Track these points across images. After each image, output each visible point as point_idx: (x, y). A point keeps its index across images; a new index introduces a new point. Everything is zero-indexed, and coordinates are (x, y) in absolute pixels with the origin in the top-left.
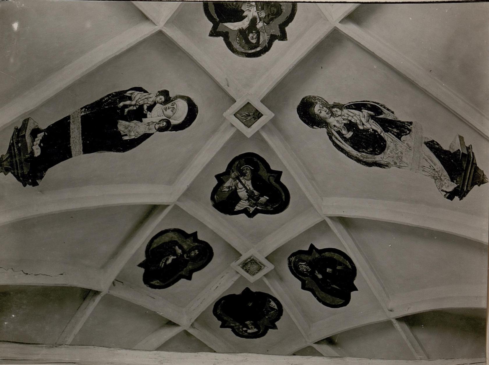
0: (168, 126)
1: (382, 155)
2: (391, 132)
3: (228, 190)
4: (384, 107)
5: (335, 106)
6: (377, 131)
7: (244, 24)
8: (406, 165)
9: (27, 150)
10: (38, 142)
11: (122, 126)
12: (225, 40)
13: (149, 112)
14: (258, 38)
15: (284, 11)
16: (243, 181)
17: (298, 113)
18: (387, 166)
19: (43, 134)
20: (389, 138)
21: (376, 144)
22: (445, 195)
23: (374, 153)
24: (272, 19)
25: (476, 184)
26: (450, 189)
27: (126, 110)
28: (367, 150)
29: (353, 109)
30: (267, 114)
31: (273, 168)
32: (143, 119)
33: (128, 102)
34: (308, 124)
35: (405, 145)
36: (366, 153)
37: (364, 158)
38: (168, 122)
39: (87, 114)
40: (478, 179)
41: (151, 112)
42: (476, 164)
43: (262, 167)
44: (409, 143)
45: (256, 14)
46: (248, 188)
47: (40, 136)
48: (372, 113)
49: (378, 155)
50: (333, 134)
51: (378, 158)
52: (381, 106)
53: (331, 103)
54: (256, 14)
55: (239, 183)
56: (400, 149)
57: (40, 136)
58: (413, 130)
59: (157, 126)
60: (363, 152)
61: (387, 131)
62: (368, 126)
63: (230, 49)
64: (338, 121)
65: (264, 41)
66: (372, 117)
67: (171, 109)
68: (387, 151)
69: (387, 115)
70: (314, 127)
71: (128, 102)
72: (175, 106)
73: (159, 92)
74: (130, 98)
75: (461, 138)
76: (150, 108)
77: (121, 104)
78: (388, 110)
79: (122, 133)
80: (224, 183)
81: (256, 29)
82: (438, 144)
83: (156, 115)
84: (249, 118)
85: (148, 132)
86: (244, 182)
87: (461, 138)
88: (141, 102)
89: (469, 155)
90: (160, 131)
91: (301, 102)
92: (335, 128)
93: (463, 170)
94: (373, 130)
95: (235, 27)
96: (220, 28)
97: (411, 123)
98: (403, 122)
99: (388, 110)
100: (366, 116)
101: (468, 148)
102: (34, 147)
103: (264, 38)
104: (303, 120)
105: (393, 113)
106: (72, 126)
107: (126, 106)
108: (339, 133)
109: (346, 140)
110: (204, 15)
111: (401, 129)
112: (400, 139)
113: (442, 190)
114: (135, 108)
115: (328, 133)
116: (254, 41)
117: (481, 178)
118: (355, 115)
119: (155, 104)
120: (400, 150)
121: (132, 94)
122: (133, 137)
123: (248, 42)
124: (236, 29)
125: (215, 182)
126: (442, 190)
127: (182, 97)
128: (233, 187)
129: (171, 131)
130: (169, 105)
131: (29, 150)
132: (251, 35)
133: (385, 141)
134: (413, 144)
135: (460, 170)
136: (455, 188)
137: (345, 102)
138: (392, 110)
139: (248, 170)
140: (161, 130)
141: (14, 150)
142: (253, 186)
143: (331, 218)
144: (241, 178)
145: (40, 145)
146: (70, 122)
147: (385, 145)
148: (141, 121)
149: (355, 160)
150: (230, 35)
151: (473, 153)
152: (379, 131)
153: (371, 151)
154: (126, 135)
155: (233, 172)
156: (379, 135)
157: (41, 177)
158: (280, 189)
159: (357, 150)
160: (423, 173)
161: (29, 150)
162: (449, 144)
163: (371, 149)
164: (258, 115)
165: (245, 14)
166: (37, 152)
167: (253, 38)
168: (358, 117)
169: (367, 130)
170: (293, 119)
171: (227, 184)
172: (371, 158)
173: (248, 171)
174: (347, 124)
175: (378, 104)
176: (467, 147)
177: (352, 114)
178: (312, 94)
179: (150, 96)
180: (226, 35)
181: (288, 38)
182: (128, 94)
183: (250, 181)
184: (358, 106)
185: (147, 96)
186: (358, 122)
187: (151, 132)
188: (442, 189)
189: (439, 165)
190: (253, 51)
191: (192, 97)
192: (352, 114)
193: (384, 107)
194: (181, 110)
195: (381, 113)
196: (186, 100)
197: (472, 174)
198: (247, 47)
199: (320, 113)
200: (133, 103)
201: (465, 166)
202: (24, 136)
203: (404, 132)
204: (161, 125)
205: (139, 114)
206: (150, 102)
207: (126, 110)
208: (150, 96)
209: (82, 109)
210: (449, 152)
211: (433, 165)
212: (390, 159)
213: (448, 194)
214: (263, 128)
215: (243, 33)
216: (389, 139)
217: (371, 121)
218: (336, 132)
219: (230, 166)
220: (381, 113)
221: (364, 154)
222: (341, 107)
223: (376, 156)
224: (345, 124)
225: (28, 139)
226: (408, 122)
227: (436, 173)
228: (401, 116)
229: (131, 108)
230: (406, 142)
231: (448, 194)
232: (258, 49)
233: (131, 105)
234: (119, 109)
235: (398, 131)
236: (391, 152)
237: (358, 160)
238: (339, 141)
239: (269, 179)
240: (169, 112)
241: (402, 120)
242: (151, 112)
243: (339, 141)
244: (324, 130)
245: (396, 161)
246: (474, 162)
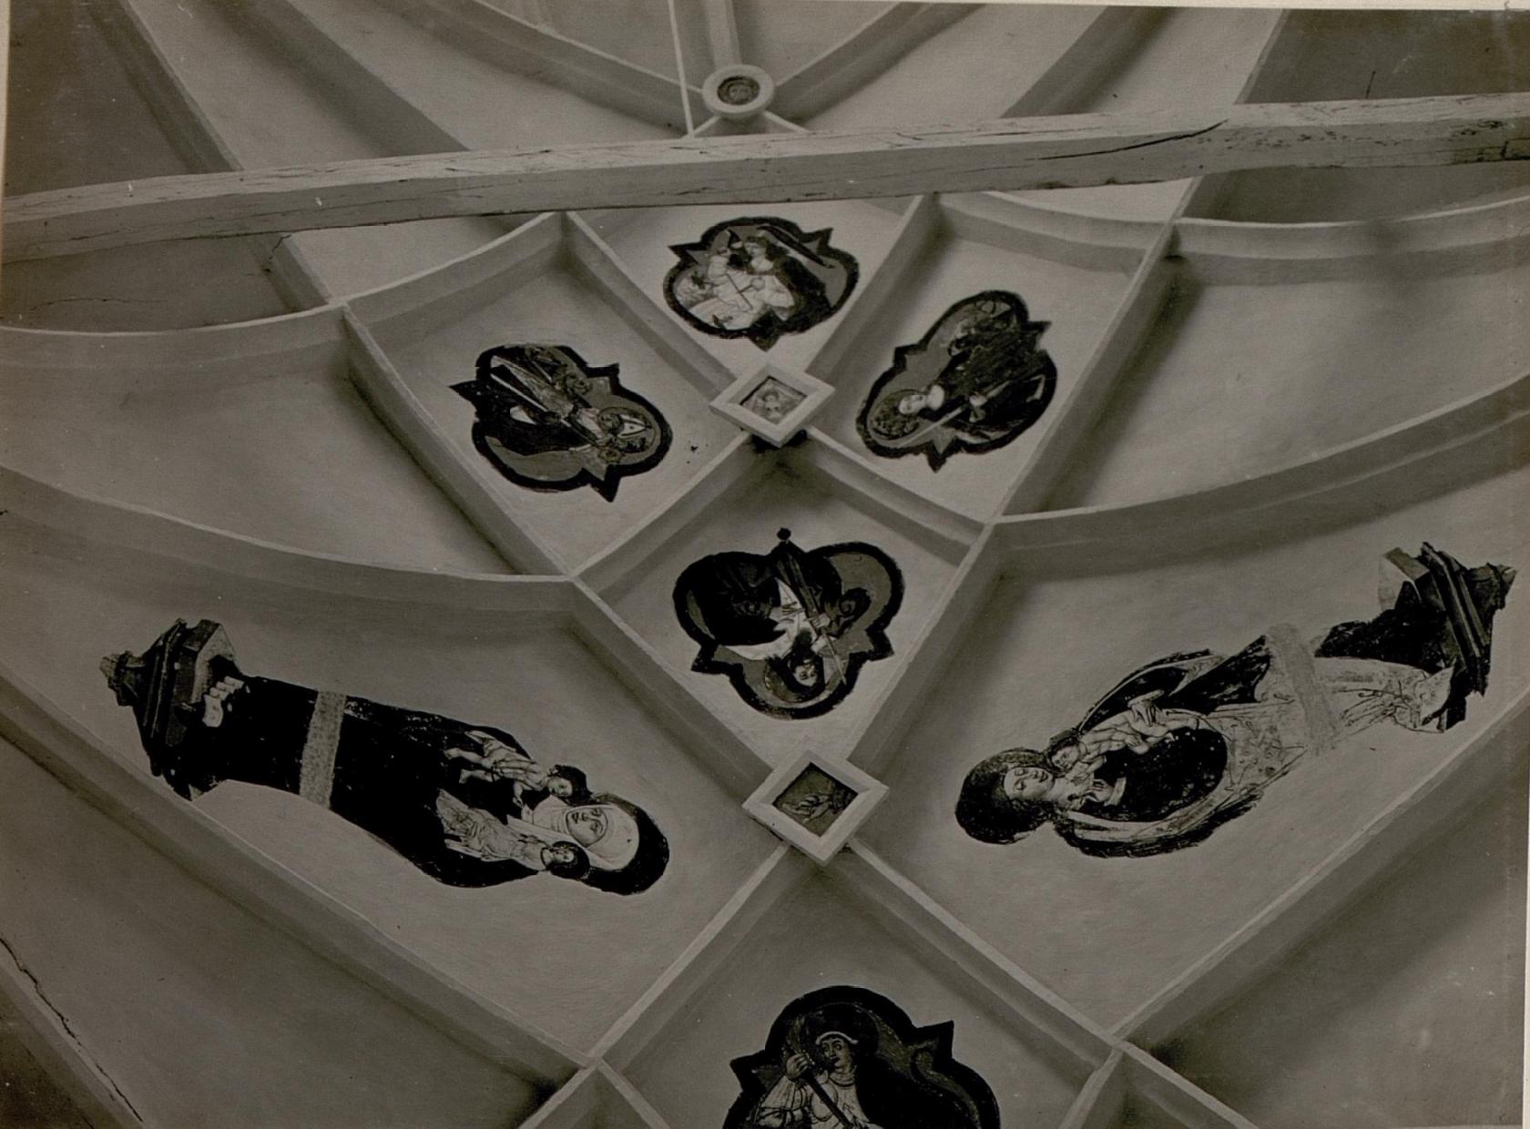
0: (577, 868)
1: (1225, 781)
2: (1223, 703)
3: (777, 1123)
4: (1182, 658)
5: (1058, 745)
6: (1186, 729)
7: (781, 647)
8: (1300, 751)
9: (190, 693)
10: (224, 696)
11: (448, 807)
12: (733, 682)
13: (526, 808)
14: (820, 672)
15: (874, 599)
16: (827, 1088)
17: (962, 824)
18: (1252, 798)
19: (239, 684)
20: (1224, 721)
21: (1198, 760)
22: (1439, 727)
23: (1202, 791)
24: (848, 624)
25: (1492, 610)
26: (1443, 695)
27: (465, 774)
28: (1178, 797)
29: (1103, 718)
30: (870, 792)
31: (918, 1022)
32: (510, 818)
33: (472, 756)
34: (995, 840)
35: (1272, 700)
36: (1180, 807)
37: (1182, 824)
38: (581, 855)
39: (358, 720)
40: (1489, 590)
41: (532, 807)
42: (1462, 568)
43: (885, 1030)
44: (1281, 690)
45: (807, 625)
46: (850, 1119)
47: (231, 684)
48: (1157, 693)
49: (1214, 787)
50: (1073, 822)
51: (1220, 796)
52: (1172, 660)
53: (1043, 746)
54: (807, 625)
55: (816, 1098)
56: (1263, 724)
57: (231, 684)
58: (1273, 651)
59: (548, 856)
60: (1173, 809)
61: (1206, 707)
62: (1157, 733)
63: (749, 703)
64: (1076, 780)
65: (836, 674)
66: (1160, 703)
67: (590, 823)
68: (1235, 758)
69: (1199, 669)
70: (1017, 835)
71: (472, 756)
72: (602, 819)
73: (558, 767)
74: (479, 749)
75: (1396, 556)
76: (534, 798)
77: (454, 752)
78: (1192, 656)
79: (447, 829)
80: (765, 1092)
81: (811, 654)
82: (1349, 626)
83: (547, 822)
84: (819, 811)
85: (520, 860)
86: (831, 1095)
87: (1396, 556)
88: (508, 773)
89: (1433, 567)
90: (555, 873)
91: (964, 789)
92: (1076, 802)
93: (1442, 616)
94: (1175, 732)
95: (758, 653)
96: (721, 654)
97: (1261, 641)
98: (1244, 653)
99: (1192, 656)
100: (1143, 711)
101: (1423, 559)
102: (208, 698)
103: (834, 668)
104: (979, 838)
105: (1206, 653)
106: (315, 719)
107: (463, 763)
108: (1091, 808)
109: (1112, 812)
110: (678, 625)
111: (1240, 675)
112: (1254, 701)
113: (1426, 721)
114: (489, 779)
115: (1059, 831)
116: (810, 682)
117: (1496, 581)
118: (1115, 729)
119: (545, 793)
120: (1264, 727)
121: (484, 740)
122: (478, 855)
123: (794, 686)
124: (761, 657)
125: (733, 1089)
126: (1426, 721)
127: (623, 804)
128: (798, 1113)
129: (586, 882)
130: (586, 810)
131: (194, 698)
132: (799, 670)
133: (1219, 736)
134: (1290, 683)
135: (1437, 624)
136: (1452, 681)
137: (1080, 714)
138: (1202, 649)
139: (837, 1045)
140: (557, 868)
141: (160, 667)
142: (865, 1110)
143: (1031, 105)
144: (821, 1079)
145: (224, 704)
146: (312, 708)
147: (1223, 743)
148: (505, 822)
149: (1160, 851)
150: (745, 671)
151: (1440, 554)
152: (1191, 723)
153: (1192, 792)
154: (457, 839)
155: (792, 1053)
156: (1198, 732)
157: (205, 788)
158: (958, 1090)
159: (1155, 816)
160: (1356, 727)
161: (194, 698)
162: (1368, 595)
163: (1190, 786)
164: (843, 795)
165: (778, 628)
166: (213, 718)
167: (805, 676)
168: (1125, 728)
169: (1160, 746)
170: (949, 839)
171: (774, 1099)
172: (1197, 813)
173: (840, 1054)
174: (1104, 765)
175: (1161, 662)
176: (1419, 559)
177: (1105, 735)
178: (986, 756)
179: (533, 767)
180: (736, 674)
181: (894, 647)
182: (475, 735)
183: (853, 1090)
184: (1115, 704)
185: (524, 765)
186: (1129, 740)
187: (529, 864)
188: (1423, 716)
189: (1377, 670)
190: (810, 703)
191: (651, 813)
192: (1105, 735)
193: (1182, 658)
194: (618, 849)
195: (1178, 674)
196: (632, 814)
197: (1468, 599)
198: (792, 696)
199: (1023, 787)
200: (487, 763)
201: (1440, 602)
202: (194, 655)
203: (1253, 675)
204: (560, 858)
205: (499, 799)
206: (536, 780)
207: (465, 774)
208: (533, 767)
209: (350, 699)
210: (1387, 614)
211: (1366, 685)
212: (1250, 772)
213: (1445, 714)
214: (860, 833)
215: (779, 668)
216: (1227, 723)
217: (1161, 714)
218: (1081, 811)
219: (779, 1031)
220: (1178, 674)
221: (1177, 813)
222: (1070, 739)
223: (1210, 797)
224: (1098, 773)
225: (201, 672)
226: (1252, 645)
227: (1386, 696)
228: (1228, 647)
229: (480, 773)
230: (1270, 694)
231: (1445, 714)
232: (823, 697)
233: (478, 766)
234: (445, 759)
235: (1240, 685)
236: (1246, 753)
237: (1167, 845)
238: (1098, 828)
239: (913, 1066)
240: (583, 829)
241: (1235, 651)
242: (532, 807)
243: (1098, 828)
244: (1048, 827)
245: (1269, 763)
246: (1456, 568)
